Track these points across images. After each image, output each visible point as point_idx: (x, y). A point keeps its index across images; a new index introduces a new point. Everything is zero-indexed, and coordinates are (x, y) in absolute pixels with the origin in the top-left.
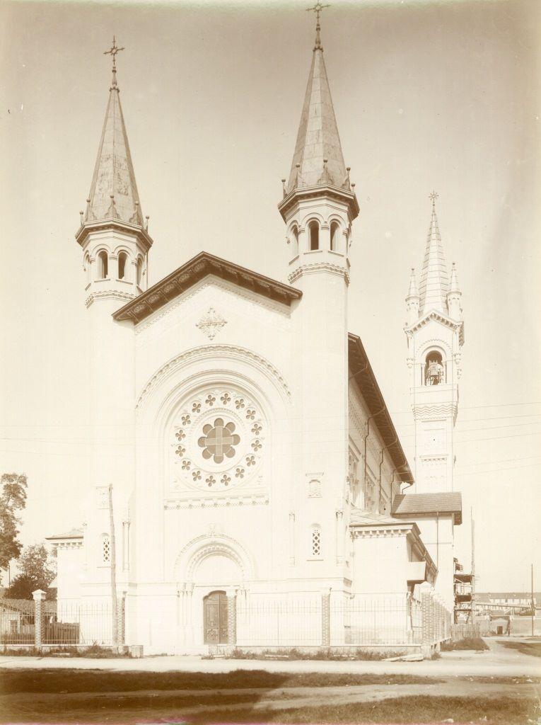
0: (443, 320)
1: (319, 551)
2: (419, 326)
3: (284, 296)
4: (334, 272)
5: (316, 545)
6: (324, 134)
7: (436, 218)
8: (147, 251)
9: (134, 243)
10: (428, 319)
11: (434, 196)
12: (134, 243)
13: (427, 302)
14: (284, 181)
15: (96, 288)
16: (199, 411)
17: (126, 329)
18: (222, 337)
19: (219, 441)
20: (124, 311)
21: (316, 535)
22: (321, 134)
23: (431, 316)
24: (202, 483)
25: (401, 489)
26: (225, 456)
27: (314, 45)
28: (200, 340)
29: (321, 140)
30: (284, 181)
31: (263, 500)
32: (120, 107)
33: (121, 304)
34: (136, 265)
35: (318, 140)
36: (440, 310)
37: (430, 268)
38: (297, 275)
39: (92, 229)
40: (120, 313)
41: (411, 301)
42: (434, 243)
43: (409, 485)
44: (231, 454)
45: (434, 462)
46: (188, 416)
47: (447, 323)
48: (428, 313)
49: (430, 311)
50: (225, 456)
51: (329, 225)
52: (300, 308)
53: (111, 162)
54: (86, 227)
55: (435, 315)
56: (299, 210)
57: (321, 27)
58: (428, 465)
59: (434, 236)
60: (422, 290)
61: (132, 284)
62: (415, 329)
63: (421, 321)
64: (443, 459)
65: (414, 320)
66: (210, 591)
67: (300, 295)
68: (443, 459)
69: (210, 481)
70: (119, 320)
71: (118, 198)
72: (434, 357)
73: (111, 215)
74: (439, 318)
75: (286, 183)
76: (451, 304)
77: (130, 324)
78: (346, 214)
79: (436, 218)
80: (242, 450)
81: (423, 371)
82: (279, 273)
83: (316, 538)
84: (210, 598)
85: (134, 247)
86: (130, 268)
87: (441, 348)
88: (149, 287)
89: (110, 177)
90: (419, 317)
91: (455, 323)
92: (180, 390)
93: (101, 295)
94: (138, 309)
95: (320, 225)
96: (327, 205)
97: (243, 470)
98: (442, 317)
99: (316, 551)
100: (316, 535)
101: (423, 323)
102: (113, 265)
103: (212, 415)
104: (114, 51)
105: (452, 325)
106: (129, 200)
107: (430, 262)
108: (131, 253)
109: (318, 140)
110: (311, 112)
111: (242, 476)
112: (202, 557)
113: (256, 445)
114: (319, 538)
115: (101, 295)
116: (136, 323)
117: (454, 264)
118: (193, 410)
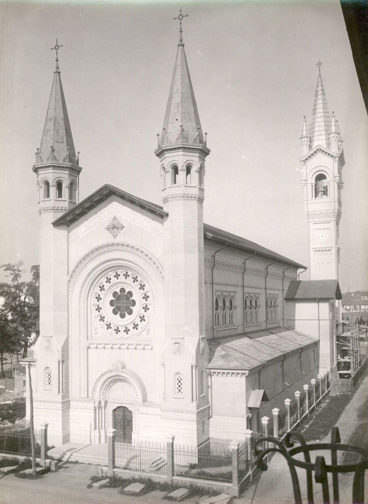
0: (326, 153)
1: (182, 391)
2: (309, 157)
3: (157, 213)
4: (189, 198)
5: (180, 386)
6: (182, 105)
7: (321, 79)
8: (78, 175)
9: (67, 174)
10: (315, 152)
11: (319, 64)
12: (67, 174)
13: (315, 139)
14: (158, 135)
15: (44, 205)
16: (104, 290)
17: (62, 232)
18: (121, 238)
19: (123, 303)
20: (59, 220)
21: (179, 380)
22: (180, 106)
23: (318, 150)
24: (112, 331)
25: (298, 273)
26: (126, 314)
27: (178, 42)
28: (107, 238)
29: (180, 110)
30: (158, 135)
31: (149, 347)
32: (60, 81)
33: (60, 215)
34: (68, 188)
35: (178, 109)
36: (324, 147)
37: (317, 115)
38: (165, 200)
39: (40, 168)
40: (57, 222)
41: (303, 139)
42: (320, 97)
43: (304, 270)
44: (130, 313)
45: (320, 253)
46: (99, 296)
47: (329, 154)
48: (315, 148)
49: (317, 147)
50: (126, 314)
51: (185, 168)
52: (168, 221)
53: (53, 121)
54: (36, 167)
55: (320, 149)
56: (165, 158)
57: (182, 30)
58: (321, 254)
59: (320, 92)
60: (311, 131)
61: (66, 201)
62: (307, 159)
63: (311, 153)
64: (329, 250)
65: (306, 152)
66: (116, 406)
67: (167, 215)
68: (329, 250)
69: (117, 331)
70: (57, 226)
71: (56, 147)
72: (320, 177)
73: (51, 159)
74: (323, 151)
75: (160, 136)
76: (331, 141)
77: (66, 227)
78: (198, 158)
79: (321, 79)
80: (137, 309)
81: (313, 188)
82: (153, 197)
83: (180, 382)
84: (118, 410)
85: (67, 176)
86: (65, 192)
87: (324, 171)
88: (80, 202)
89: (52, 132)
90: (310, 150)
91: (335, 155)
92: (87, 282)
93: (46, 210)
94: (68, 219)
95: (179, 168)
96: (183, 155)
97: (137, 325)
98: (326, 150)
99: (180, 391)
100: (179, 380)
101: (312, 155)
102: (53, 191)
103: (117, 286)
104: (57, 47)
105: (332, 156)
106: (64, 146)
107: (318, 111)
108: (64, 180)
109: (178, 109)
110: (175, 90)
111: (144, 320)
112: (108, 387)
113: (146, 308)
114: (181, 382)
115: (46, 210)
116: (68, 226)
117: (333, 112)
118: (101, 290)
